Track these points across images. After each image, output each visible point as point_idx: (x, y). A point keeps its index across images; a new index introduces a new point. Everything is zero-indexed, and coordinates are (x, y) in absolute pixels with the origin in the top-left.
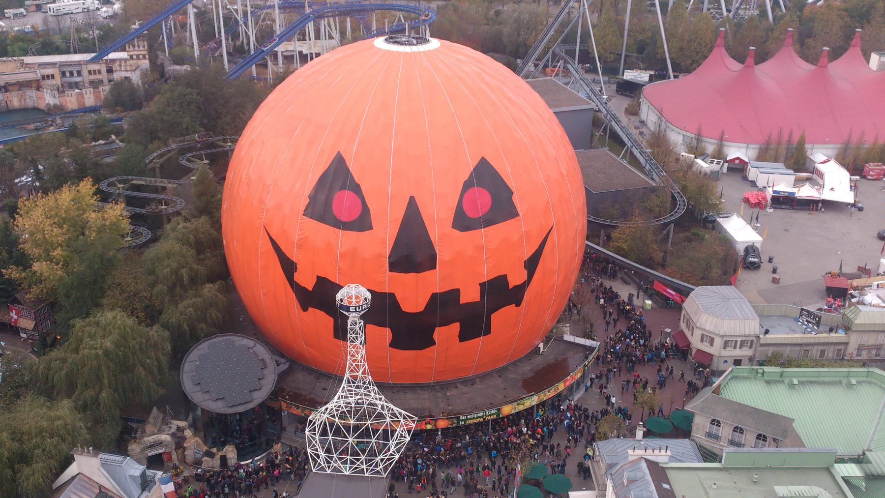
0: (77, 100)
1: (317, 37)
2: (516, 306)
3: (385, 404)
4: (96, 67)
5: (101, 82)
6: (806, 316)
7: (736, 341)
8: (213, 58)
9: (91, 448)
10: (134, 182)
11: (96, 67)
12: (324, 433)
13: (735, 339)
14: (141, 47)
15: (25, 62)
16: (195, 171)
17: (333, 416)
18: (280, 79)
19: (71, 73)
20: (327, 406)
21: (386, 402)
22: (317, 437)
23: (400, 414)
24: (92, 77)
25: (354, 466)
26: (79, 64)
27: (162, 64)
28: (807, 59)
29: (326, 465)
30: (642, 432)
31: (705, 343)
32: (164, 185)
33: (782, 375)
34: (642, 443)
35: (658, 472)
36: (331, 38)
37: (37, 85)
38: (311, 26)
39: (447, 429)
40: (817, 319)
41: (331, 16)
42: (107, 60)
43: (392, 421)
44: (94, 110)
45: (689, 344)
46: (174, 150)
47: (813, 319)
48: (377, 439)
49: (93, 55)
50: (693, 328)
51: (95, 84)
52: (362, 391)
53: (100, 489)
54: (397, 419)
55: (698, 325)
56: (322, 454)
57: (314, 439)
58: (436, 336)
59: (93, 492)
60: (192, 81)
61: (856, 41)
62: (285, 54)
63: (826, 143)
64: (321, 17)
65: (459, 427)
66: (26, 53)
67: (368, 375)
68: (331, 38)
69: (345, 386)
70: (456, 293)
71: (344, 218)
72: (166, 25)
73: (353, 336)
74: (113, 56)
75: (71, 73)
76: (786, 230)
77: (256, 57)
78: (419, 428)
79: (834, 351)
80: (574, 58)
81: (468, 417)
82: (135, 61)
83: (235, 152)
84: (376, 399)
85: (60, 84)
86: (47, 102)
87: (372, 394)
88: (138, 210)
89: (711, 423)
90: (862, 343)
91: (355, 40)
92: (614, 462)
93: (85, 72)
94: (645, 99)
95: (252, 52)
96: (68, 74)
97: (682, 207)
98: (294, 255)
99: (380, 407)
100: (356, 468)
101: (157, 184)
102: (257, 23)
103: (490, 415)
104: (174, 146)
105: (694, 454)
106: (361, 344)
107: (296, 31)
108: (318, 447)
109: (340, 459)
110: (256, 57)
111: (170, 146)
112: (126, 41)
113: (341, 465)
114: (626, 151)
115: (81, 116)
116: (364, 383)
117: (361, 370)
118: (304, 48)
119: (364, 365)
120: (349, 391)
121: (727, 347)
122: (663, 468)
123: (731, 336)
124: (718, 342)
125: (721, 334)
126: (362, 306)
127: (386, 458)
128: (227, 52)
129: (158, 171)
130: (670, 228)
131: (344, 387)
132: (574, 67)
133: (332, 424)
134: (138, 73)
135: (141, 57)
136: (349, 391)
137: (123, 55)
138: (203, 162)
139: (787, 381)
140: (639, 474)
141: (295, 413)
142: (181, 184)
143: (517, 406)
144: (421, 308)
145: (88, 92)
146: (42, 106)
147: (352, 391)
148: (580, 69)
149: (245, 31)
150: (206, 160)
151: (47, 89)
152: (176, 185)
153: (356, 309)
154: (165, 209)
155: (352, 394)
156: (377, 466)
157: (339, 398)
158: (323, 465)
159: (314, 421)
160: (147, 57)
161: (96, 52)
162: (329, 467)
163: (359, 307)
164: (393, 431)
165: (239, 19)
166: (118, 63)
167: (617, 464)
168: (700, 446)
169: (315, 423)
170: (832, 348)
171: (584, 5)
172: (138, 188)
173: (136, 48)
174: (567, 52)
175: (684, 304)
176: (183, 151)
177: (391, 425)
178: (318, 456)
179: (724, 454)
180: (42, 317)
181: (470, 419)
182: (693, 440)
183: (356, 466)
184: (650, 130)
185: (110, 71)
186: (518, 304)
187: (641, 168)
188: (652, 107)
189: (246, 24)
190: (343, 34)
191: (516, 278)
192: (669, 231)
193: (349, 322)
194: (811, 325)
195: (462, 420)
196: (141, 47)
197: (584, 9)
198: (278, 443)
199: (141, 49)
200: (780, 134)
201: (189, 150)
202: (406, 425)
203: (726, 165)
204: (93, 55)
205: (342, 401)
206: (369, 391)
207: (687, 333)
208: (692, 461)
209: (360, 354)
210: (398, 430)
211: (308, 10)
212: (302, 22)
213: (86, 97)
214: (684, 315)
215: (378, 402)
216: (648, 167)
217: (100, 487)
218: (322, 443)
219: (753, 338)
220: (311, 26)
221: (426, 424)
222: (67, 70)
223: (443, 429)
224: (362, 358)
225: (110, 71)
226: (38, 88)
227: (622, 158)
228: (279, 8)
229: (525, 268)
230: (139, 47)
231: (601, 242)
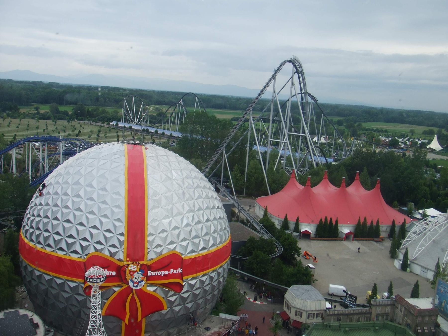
6: (349, 298)
7: (314, 314)
28: (335, 185)
31: (298, 316)
33: (340, 326)
40: (355, 299)
45: (289, 318)
47: (353, 299)
50: (291, 308)
55: (293, 306)
61: (357, 177)
63: (348, 224)
67: (103, 328)
76: (333, 265)
79: (365, 318)
80: (220, 182)
90: (378, 312)
117: (98, 324)
121: (310, 318)
123: (311, 311)
124: (305, 315)
138: (11, 222)
139: (343, 330)
150: (13, 221)
153: (97, 280)
170: (363, 316)
171: (225, 157)
175: (285, 296)
183: (94, 325)
188: (262, 207)
194: (352, 303)
197: (225, 158)
200: (326, 219)
207: (287, 311)
214: (286, 302)
219: (323, 312)
227: (249, 227)
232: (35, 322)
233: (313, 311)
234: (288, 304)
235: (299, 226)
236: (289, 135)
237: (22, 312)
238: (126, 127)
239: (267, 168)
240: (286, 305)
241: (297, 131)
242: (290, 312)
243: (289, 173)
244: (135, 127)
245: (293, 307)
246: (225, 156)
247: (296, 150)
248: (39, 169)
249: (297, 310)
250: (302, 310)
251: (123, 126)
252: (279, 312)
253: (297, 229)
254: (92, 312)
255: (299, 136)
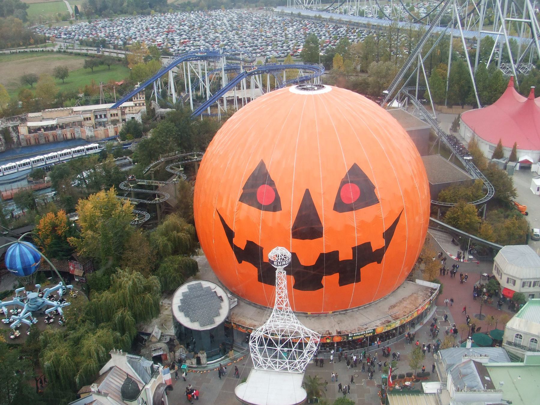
0: (105, 132)
1: (248, 87)
2: (378, 263)
3: (300, 326)
4: (114, 112)
5: (118, 121)
7: (531, 282)
8: (184, 104)
9: (121, 350)
10: (139, 183)
11: (114, 112)
12: (261, 344)
13: (530, 281)
14: (142, 98)
15: (74, 110)
16: (175, 175)
17: (267, 333)
18: (226, 116)
19: (101, 116)
20: (263, 327)
21: (300, 324)
22: (257, 346)
23: (310, 332)
24: (113, 118)
25: (282, 366)
26: (105, 110)
27: (154, 109)
29: (264, 365)
30: (470, 343)
31: (509, 284)
32: (157, 185)
34: (470, 350)
35: (482, 370)
36: (257, 87)
37: (80, 124)
38: (244, 81)
39: (340, 342)
41: (257, 74)
42: (121, 107)
43: (305, 337)
44: (114, 139)
46: (162, 162)
48: (295, 348)
49: (113, 104)
50: (502, 274)
51: (114, 122)
52: (286, 317)
53: (127, 376)
54: (307, 336)
55: (505, 272)
56: (261, 357)
57: (255, 348)
58: (324, 282)
59: (123, 378)
60: (173, 118)
62: (227, 99)
64: (251, 74)
65: (349, 341)
66: (74, 105)
68: (257, 87)
69: (275, 314)
70: (336, 253)
71: (264, 203)
72: (156, 84)
73: (280, 281)
74: (125, 104)
75: (101, 116)
77: (210, 102)
78: (322, 342)
81: (354, 335)
82: (138, 107)
83: (202, 165)
84: (295, 322)
85: (94, 123)
86: (87, 134)
87: (292, 319)
88: (142, 201)
89: (516, 337)
91: (273, 88)
92: (452, 363)
93: (109, 116)
94: (479, 138)
95: (208, 99)
96: (99, 117)
97: (491, 193)
98: (234, 228)
99: (297, 327)
100: (283, 367)
101: (153, 184)
102: (210, 81)
103: (368, 333)
104: (162, 160)
105: (505, 357)
106: (284, 286)
107: (234, 83)
108: (257, 353)
109: (273, 361)
110: (210, 102)
111: (160, 159)
112: (133, 95)
113: (273, 365)
114: (452, 156)
115: (107, 142)
116: (287, 312)
118: (242, 94)
119: (286, 300)
120: (277, 317)
122: (485, 366)
124: (519, 283)
125: (520, 277)
126: (282, 262)
127: (302, 361)
128: (193, 99)
129: (153, 176)
130: (484, 207)
131: (273, 315)
132: (415, 101)
133: (266, 339)
134: (140, 114)
135: (141, 104)
136: (277, 317)
137: (131, 104)
140: (469, 371)
141: (242, 331)
142: (167, 184)
143: (386, 328)
144: (313, 263)
145: (111, 128)
146: (84, 137)
147: (279, 317)
148: (419, 103)
149: (204, 86)
151: (87, 126)
152: (164, 185)
154: (158, 200)
155: (279, 319)
156: (295, 366)
157: (270, 322)
158: (261, 365)
159: (254, 336)
160: (145, 104)
161: (115, 102)
162: (265, 366)
163: (280, 262)
164: (306, 344)
165: (200, 78)
166: (128, 109)
167: (454, 364)
168: (508, 352)
169: (255, 338)
171: (420, 61)
172: (141, 187)
173: (139, 99)
174: (410, 92)
176: (168, 162)
177: (304, 340)
178: (258, 359)
179: (526, 356)
180: (88, 269)
181: (356, 336)
182: (504, 348)
183: (282, 366)
184: (467, 142)
185: (123, 113)
186: (379, 262)
187: (463, 168)
189: (204, 81)
190: (264, 86)
191: (377, 243)
192: (483, 210)
193: (277, 272)
195: (350, 337)
196: (142, 98)
198: (231, 350)
199: (142, 99)
201: (172, 161)
202: (314, 340)
203: (518, 164)
204: (113, 104)
205: (272, 324)
206: (290, 318)
207: (498, 277)
208: (504, 361)
209: (284, 293)
210: (309, 343)
211: (242, 71)
212: (239, 78)
213: (109, 130)
215: (295, 325)
216: (467, 167)
217: (127, 374)
218: (261, 350)
220: (244, 81)
221: (326, 339)
222: (98, 114)
223: (338, 343)
224: (285, 296)
225: (123, 113)
226: (82, 126)
227: (450, 160)
228: (225, 70)
229: (384, 237)
230: (140, 98)
231: (438, 217)
232: (219, 295)
233: (529, 279)
234: (498, 269)
235: (516, 152)
236: (507, 22)
237: (205, 284)
238: (294, 13)
239: (476, 69)
240: (496, 269)
241: (520, 15)
242: (501, 278)
243: (505, 73)
244: (304, 13)
245: (505, 274)
246: (421, 61)
247: (517, 32)
248: (199, 87)
249: (510, 277)
250: (515, 277)
251: (290, 12)
252: (485, 275)
253: (513, 158)
254: (277, 292)
255: (520, 23)
